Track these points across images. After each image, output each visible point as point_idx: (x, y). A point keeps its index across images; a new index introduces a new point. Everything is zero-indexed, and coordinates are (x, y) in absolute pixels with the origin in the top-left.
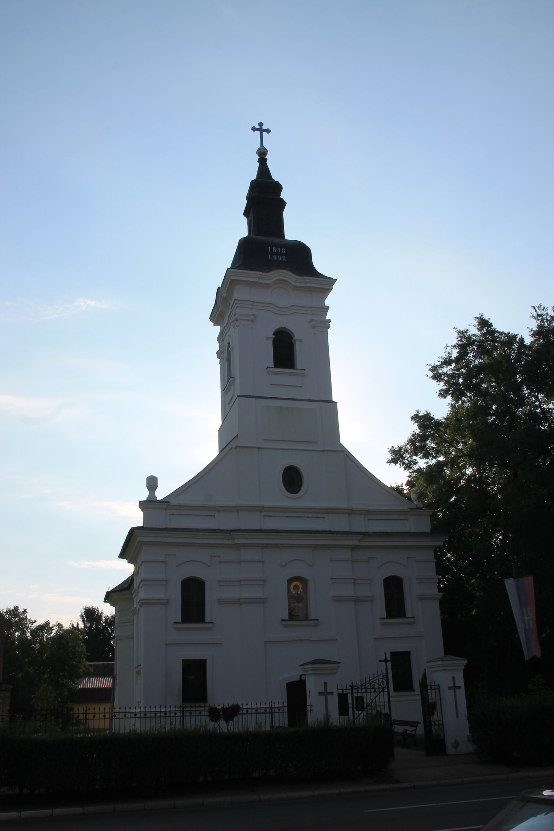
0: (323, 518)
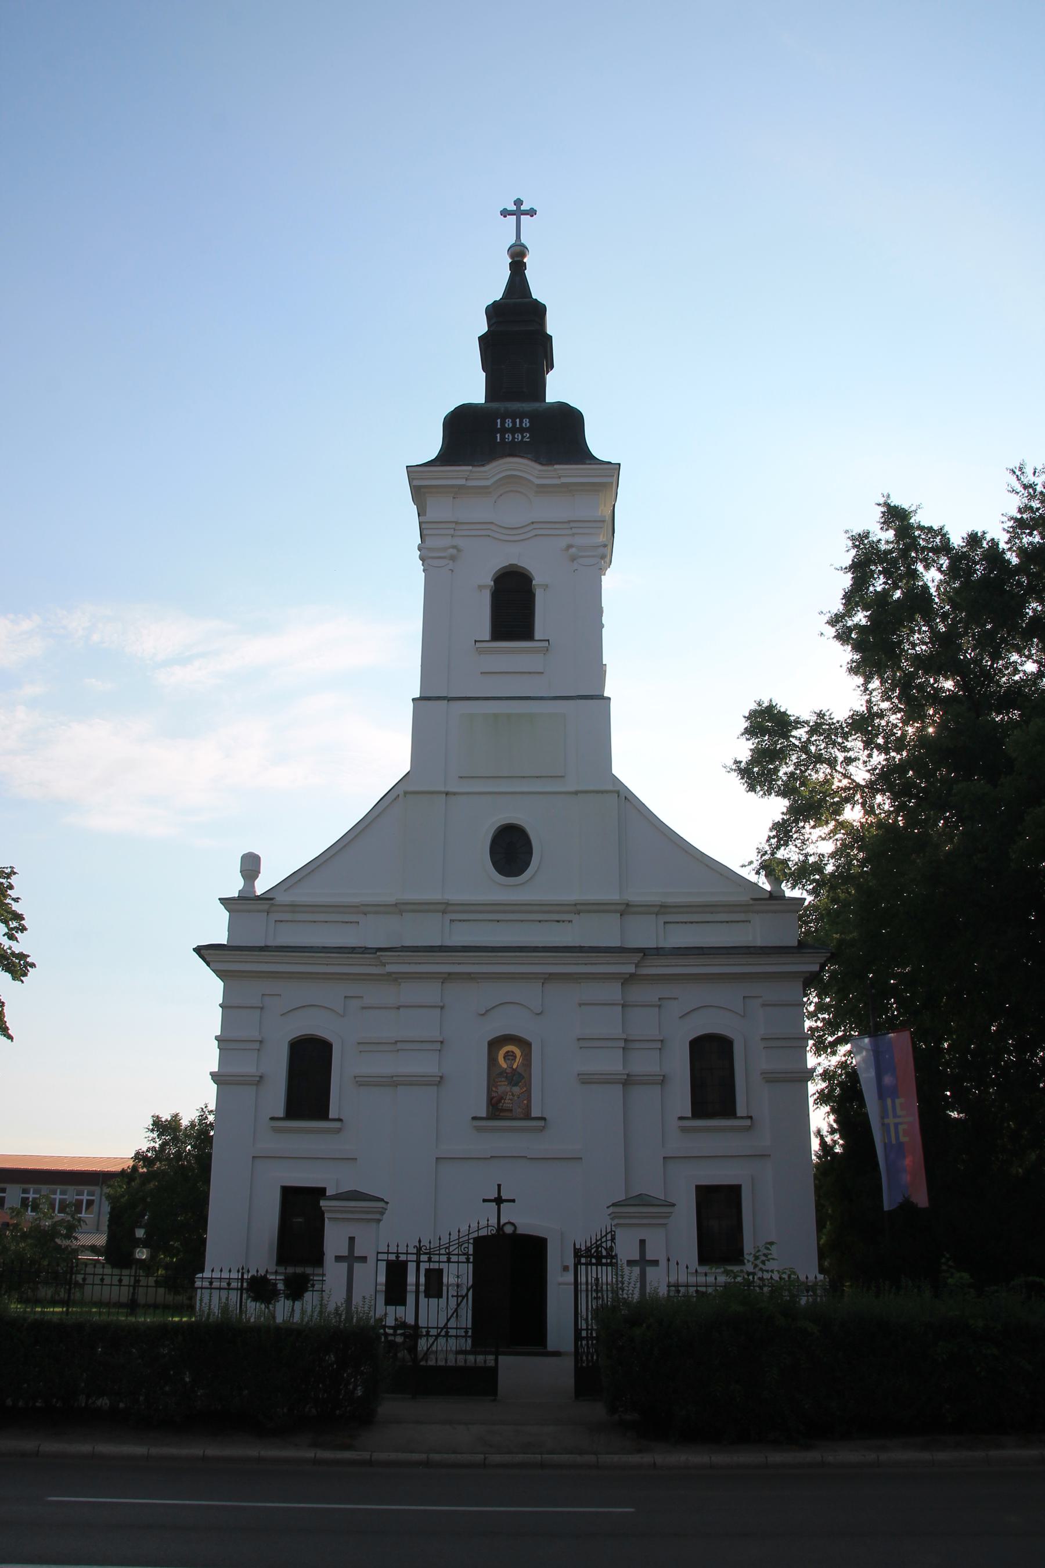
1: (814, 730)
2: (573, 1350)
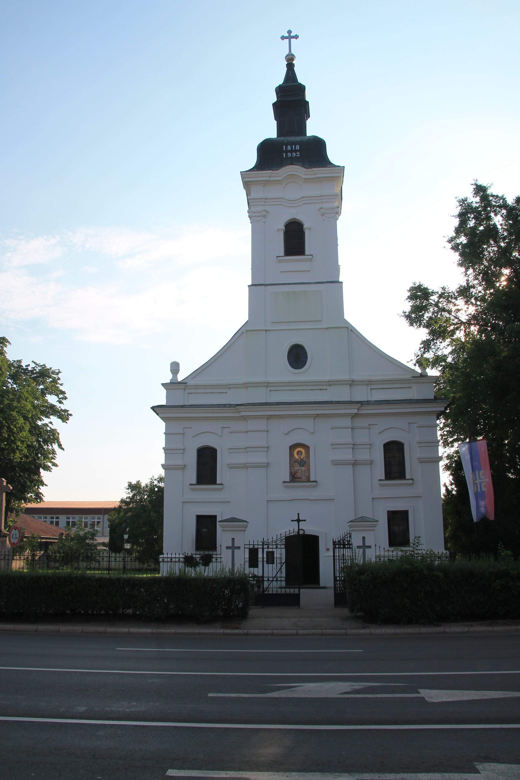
0: (326, 389)
1: (440, 296)
2: (333, 586)
